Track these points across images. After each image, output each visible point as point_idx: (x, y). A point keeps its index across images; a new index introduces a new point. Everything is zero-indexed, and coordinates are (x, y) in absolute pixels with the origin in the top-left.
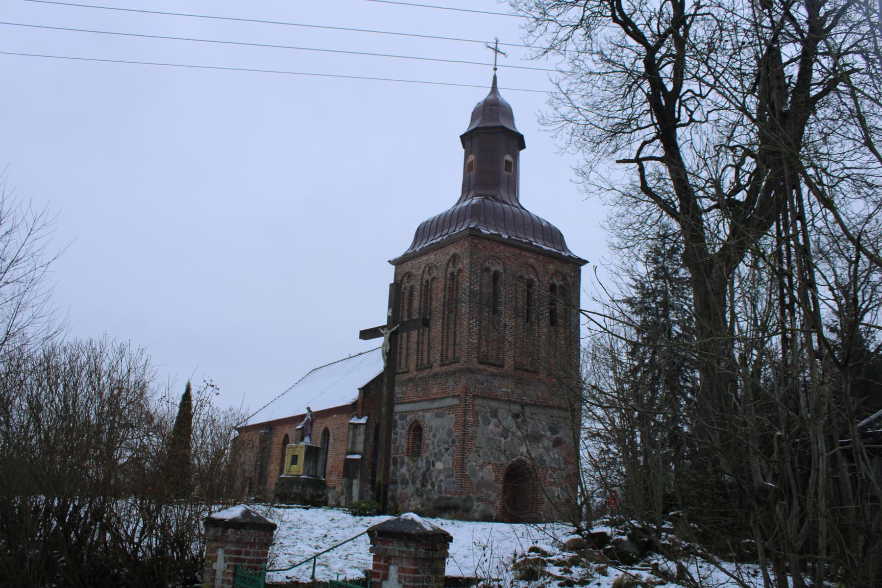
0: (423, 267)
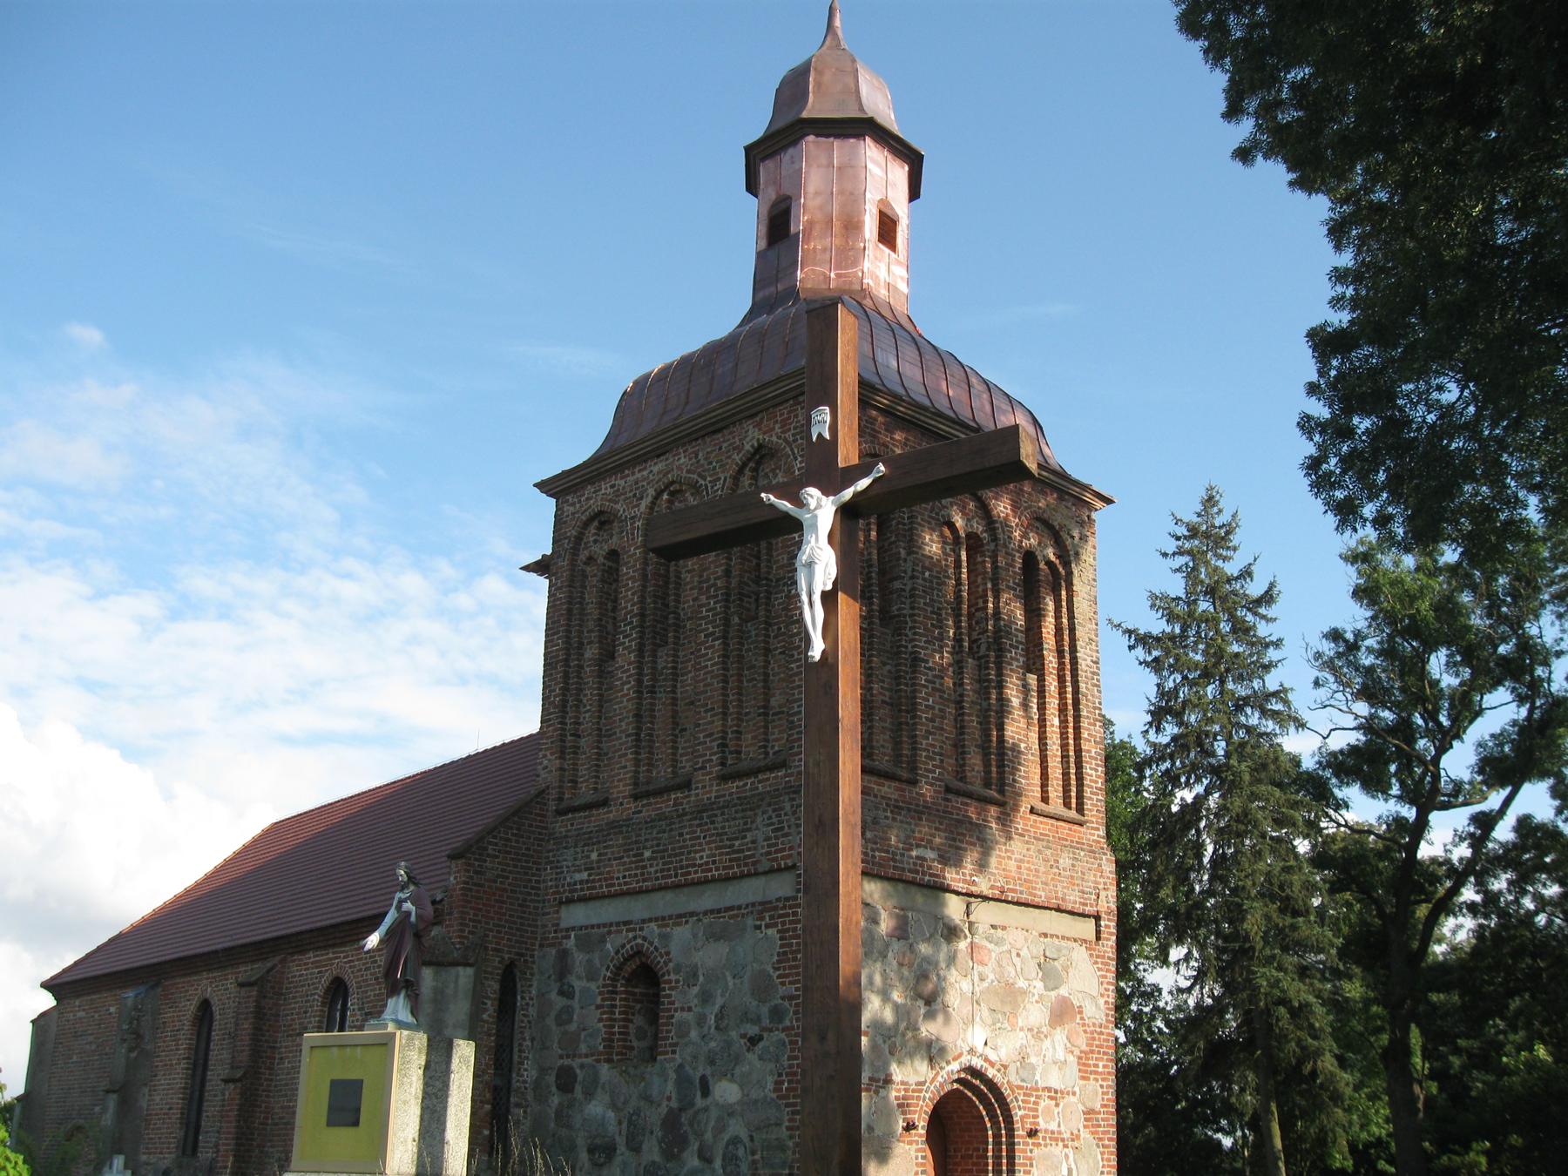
0: (651, 492)
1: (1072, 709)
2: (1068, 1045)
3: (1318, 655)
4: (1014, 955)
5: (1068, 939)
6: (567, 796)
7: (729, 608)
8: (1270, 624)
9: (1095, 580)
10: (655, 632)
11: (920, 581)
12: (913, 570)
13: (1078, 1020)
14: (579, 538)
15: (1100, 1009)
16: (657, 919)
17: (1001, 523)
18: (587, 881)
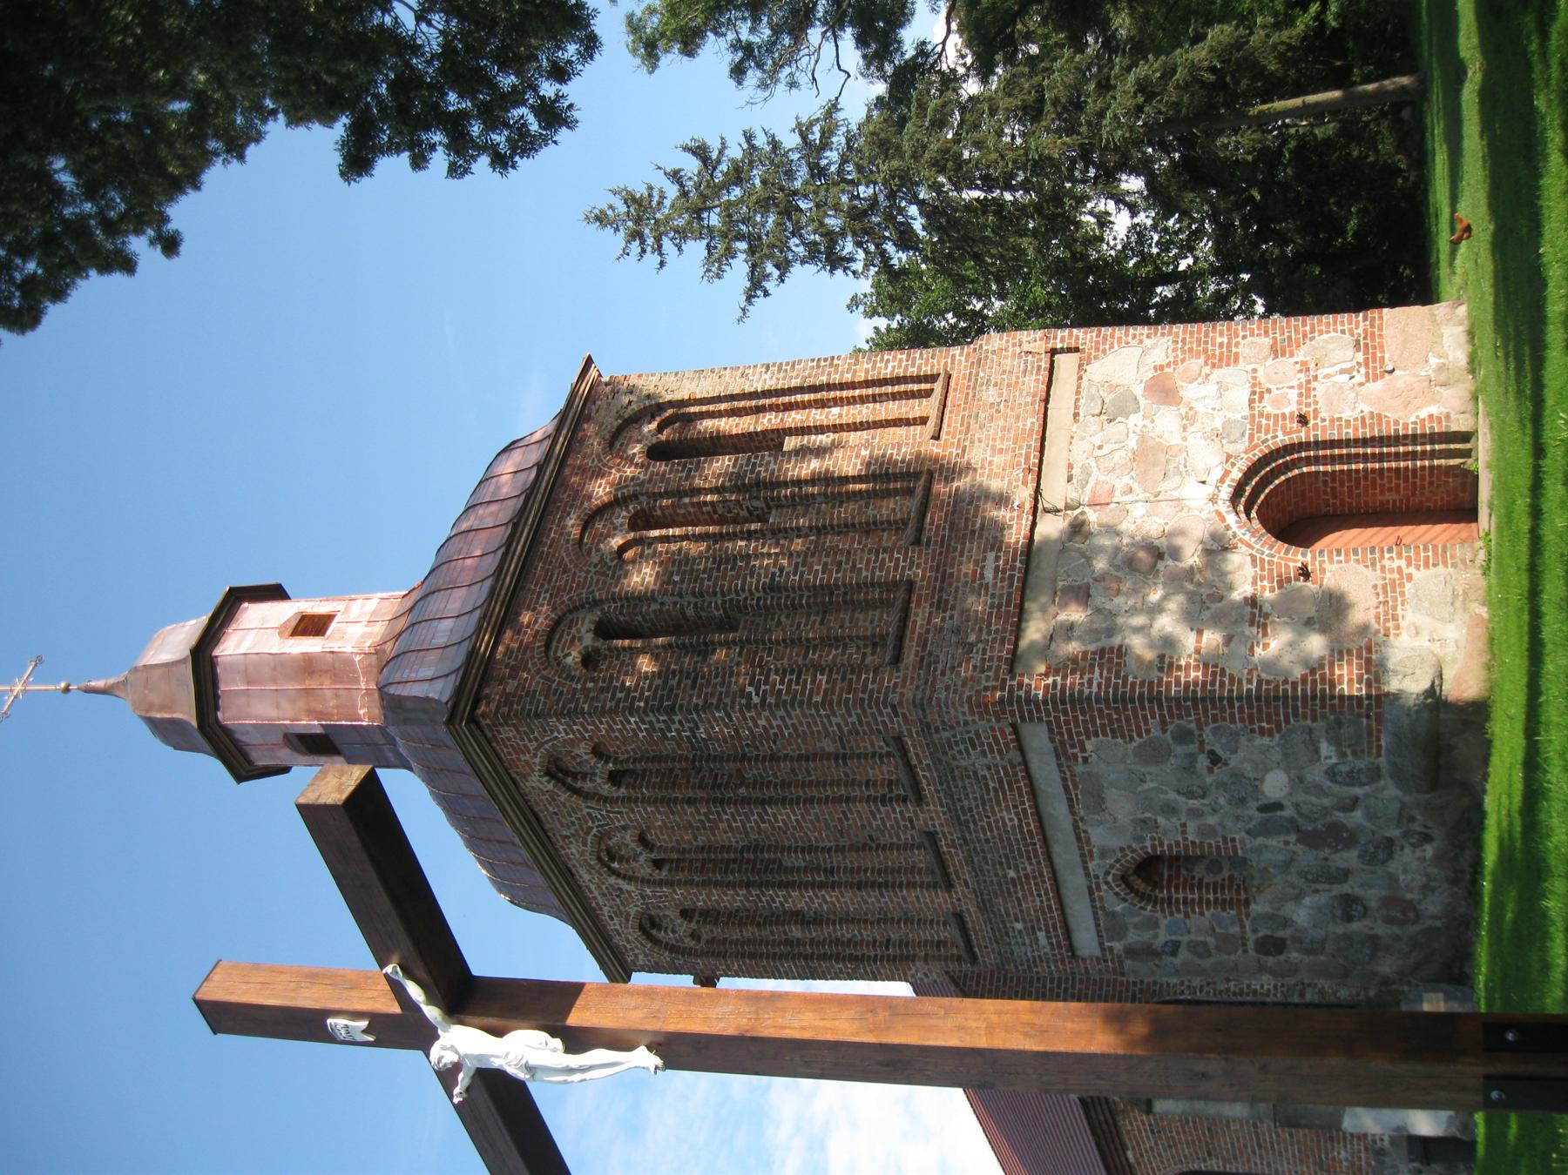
0: (612, 880)
1: (821, 393)
2: (1200, 380)
3: (763, 85)
4: (1100, 453)
5: (1079, 387)
6: (955, 952)
7: (730, 798)
8: (728, 144)
9: (676, 374)
10: (766, 871)
11: (684, 586)
12: (672, 595)
13: (1170, 370)
14: (672, 949)
15: (1156, 344)
16: (1084, 862)
17: (617, 490)
18: (1047, 932)
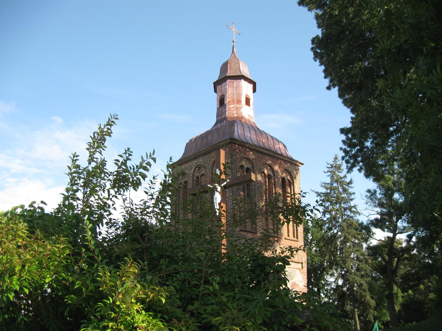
0: (194, 168)
